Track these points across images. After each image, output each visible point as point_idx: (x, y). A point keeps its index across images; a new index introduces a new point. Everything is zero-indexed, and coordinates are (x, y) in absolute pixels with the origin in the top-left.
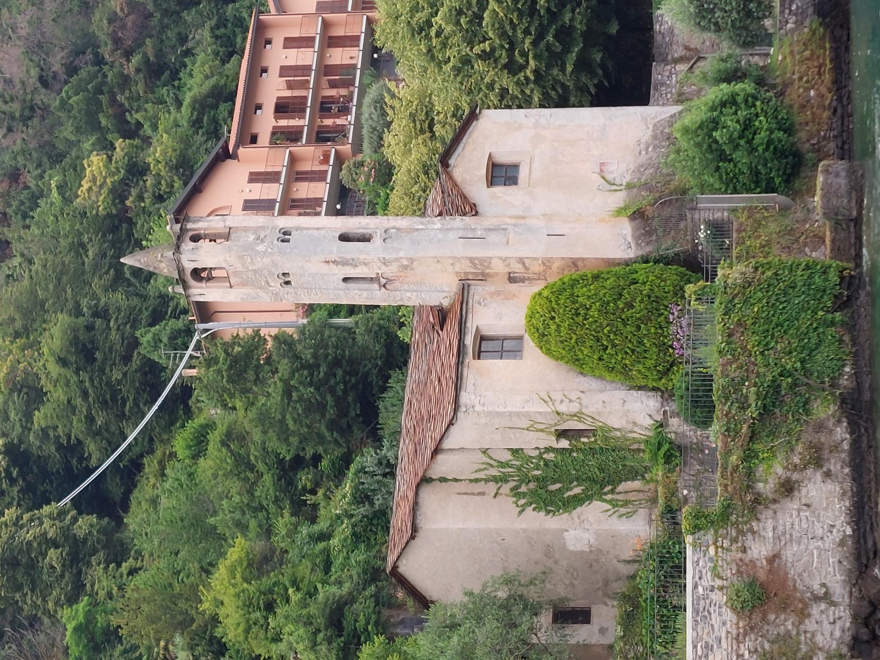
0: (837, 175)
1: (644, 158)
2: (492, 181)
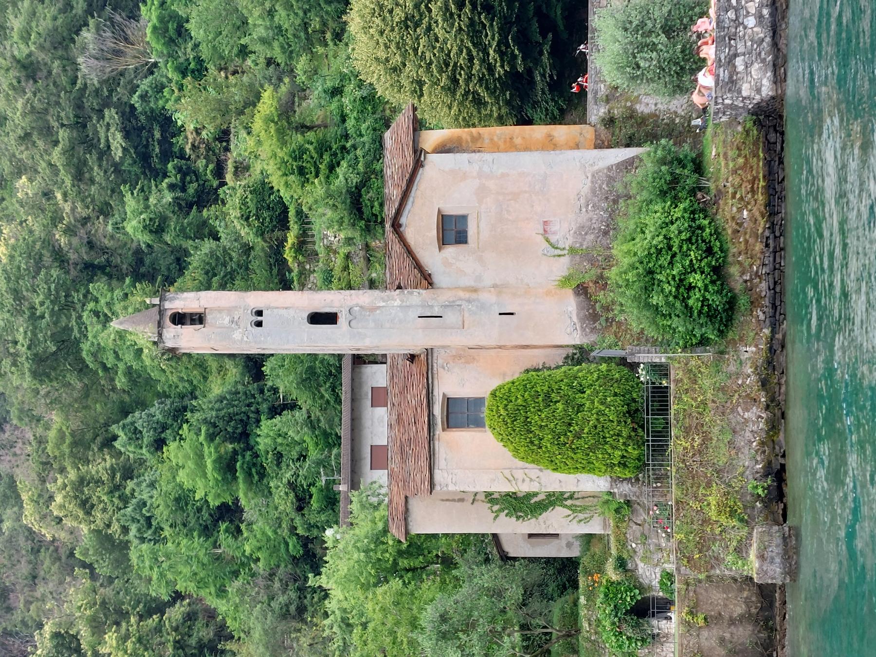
0: (772, 562)
1: (583, 218)
2: (443, 242)
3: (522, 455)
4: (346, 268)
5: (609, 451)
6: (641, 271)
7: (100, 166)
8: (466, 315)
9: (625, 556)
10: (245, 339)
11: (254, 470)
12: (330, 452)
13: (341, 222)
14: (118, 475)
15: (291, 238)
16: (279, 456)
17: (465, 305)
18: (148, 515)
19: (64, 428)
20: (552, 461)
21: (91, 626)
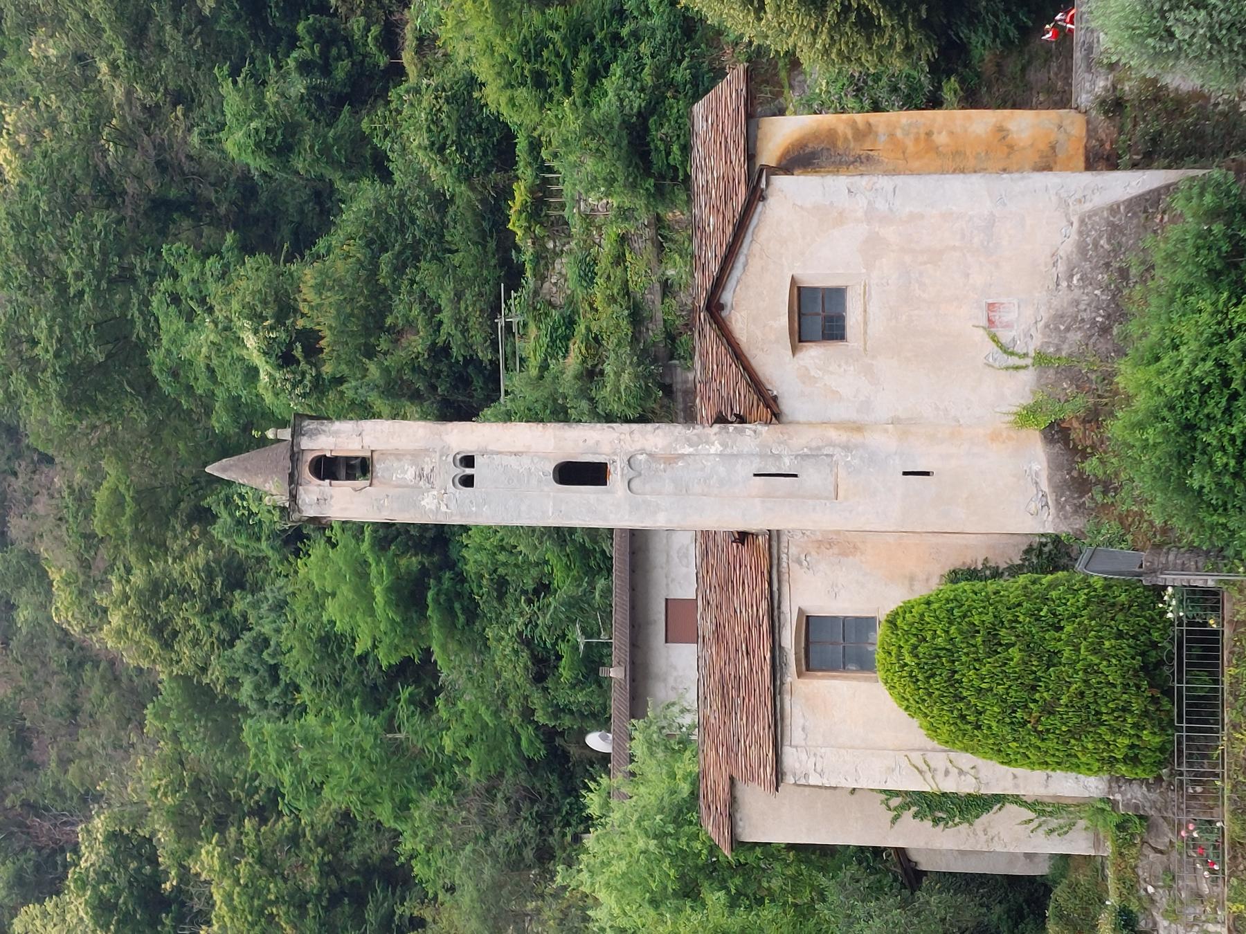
1: (1063, 299)
2: (800, 336)
3: (945, 737)
4: (619, 260)
5: (1107, 738)
6: (1170, 425)
7: (176, 24)
8: (842, 473)
9: (1134, 907)
10: (444, 508)
11: (457, 606)
12: (592, 585)
13: (611, 181)
14: (219, 582)
15: (521, 193)
16: (501, 585)
17: (838, 454)
18: (272, 662)
19: (122, 488)
20: (999, 751)
21: (175, 825)
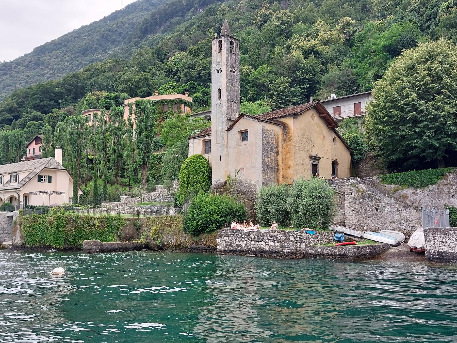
1: (244, 182)
